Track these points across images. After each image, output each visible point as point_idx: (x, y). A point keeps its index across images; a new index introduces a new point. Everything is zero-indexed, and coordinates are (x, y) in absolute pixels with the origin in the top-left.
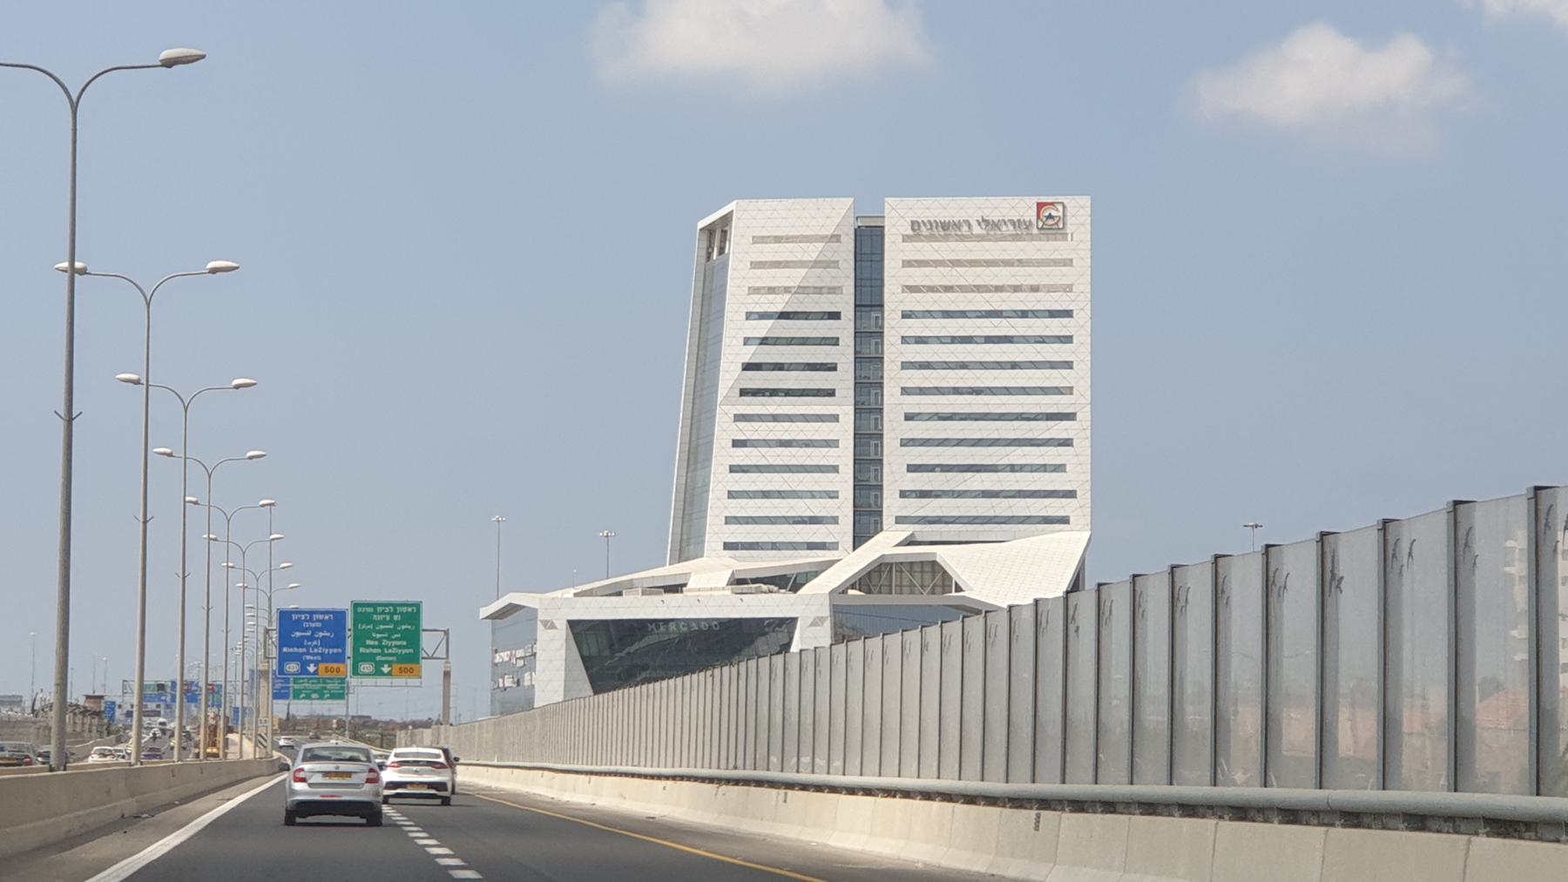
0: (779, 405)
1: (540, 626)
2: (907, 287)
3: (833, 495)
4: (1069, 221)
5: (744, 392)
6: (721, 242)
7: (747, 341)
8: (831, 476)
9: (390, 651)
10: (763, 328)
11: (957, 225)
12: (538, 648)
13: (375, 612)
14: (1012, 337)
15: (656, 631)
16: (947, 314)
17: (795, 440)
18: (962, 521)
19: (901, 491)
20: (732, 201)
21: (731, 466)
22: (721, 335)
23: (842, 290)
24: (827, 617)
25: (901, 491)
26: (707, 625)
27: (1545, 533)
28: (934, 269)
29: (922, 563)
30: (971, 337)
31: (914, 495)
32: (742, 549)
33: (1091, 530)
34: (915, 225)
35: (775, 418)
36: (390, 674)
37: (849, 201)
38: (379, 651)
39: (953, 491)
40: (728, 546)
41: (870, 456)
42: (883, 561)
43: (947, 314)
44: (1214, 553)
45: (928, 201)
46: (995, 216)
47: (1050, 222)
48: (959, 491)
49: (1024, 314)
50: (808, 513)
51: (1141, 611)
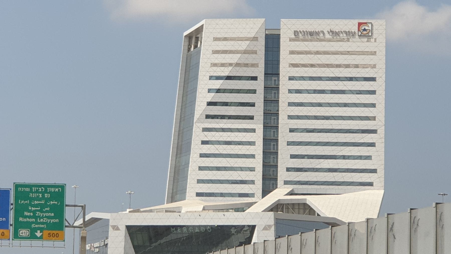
1: (110, 229)
2: (291, 64)
3: (252, 169)
4: (375, 32)
5: (208, 117)
7: (210, 91)
9: (42, 220)
10: (218, 84)
11: (318, 33)
12: (109, 241)
13: (31, 191)
15: (175, 231)
16: (312, 79)
19: (287, 168)
22: (196, 88)
24: (272, 225)
25: (287, 168)
26: (204, 229)
27: (413, 225)
28: (306, 55)
29: (299, 204)
31: (294, 170)
32: (205, 196)
33: (384, 189)
34: (296, 33)
35: (223, 130)
36: (41, 238)
37: (264, 19)
40: (198, 195)
41: (270, 150)
42: (279, 203)
43: (312, 79)
44: (366, 218)
46: (337, 29)
47: (365, 32)
49: (351, 79)
50: (240, 179)
51: (335, 240)
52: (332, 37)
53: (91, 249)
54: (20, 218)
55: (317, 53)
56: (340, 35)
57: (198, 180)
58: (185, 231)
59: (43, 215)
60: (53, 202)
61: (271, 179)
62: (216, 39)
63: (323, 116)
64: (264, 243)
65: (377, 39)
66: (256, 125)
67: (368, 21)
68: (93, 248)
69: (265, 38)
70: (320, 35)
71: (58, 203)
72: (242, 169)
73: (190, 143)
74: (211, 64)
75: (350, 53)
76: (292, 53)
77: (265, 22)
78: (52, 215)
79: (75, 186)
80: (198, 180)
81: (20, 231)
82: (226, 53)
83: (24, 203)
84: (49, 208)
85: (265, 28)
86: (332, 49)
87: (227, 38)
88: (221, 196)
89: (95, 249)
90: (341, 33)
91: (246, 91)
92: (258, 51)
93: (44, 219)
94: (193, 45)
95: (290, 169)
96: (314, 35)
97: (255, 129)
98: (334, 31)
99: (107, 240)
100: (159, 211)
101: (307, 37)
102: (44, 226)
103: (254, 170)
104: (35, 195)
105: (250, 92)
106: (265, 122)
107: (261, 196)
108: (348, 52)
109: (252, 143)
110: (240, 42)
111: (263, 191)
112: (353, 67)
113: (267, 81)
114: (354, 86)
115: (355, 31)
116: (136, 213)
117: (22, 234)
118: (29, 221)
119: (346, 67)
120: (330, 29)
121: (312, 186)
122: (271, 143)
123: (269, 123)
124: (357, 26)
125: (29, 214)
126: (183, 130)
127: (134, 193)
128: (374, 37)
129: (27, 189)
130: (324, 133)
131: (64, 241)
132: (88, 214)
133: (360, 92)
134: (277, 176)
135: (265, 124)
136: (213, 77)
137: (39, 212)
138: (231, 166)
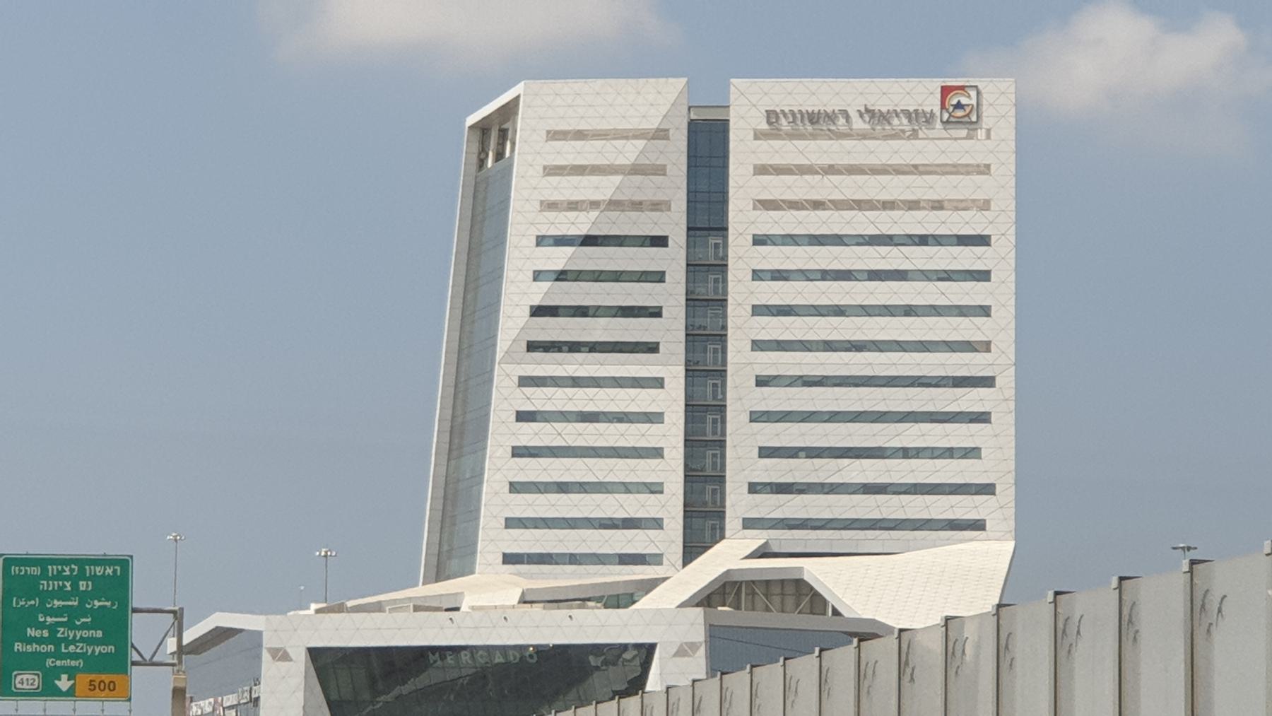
0: (581, 365)
1: (266, 656)
2: (759, 201)
3: (655, 489)
4: (986, 111)
5: (532, 347)
6: (498, 144)
7: (538, 276)
8: (653, 462)
9: (72, 648)
10: (560, 258)
11: (831, 117)
12: (263, 691)
13: (44, 575)
14: (906, 272)
15: (439, 663)
17: (603, 413)
18: (834, 526)
20: (520, 82)
21: (513, 448)
22: (502, 268)
23: (670, 206)
24: (701, 643)
29: (782, 581)
30: (850, 272)
34: (772, 116)
35: (576, 382)
36: (71, 693)
37: (684, 80)
38: (51, 648)
39: (822, 485)
40: (509, 559)
42: (727, 580)
45: (790, 84)
46: (883, 106)
47: (960, 113)
48: (832, 484)
49: (923, 240)
51: (1008, 658)
52: (869, 127)
53: (216, 710)
54: (16, 644)
55: (831, 170)
56: (891, 122)
57: (507, 519)
58: (467, 662)
59: (75, 636)
60: (99, 601)
61: (706, 515)
62: (554, 135)
63: (849, 341)
64: (666, 695)
65: (992, 133)
66: (665, 368)
67: (968, 81)
68: (221, 708)
69: (689, 131)
70: (838, 121)
71: (113, 604)
72: (627, 488)
73: (487, 416)
74: (542, 202)
75: (921, 169)
76: (761, 170)
77: (688, 87)
78: (97, 636)
79: (174, 534)
80: (507, 519)
81: (16, 676)
82: (582, 174)
83: (27, 606)
84: (91, 616)
85: (688, 103)
86: (873, 160)
87: (586, 133)
88: (571, 563)
89: (227, 712)
90: (894, 115)
91: (639, 276)
92: (668, 168)
93: (78, 644)
94: (493, 151)
95: (759, 488)
96: (822, 123)
97: (662, 379)
98: (876, 111)
99: (258, 686)
100: (397, 606)
101: (801, 128)
102: (78, 662)
103: (661, 489)
104: (54, 585)
105: (649, 279)
106: (689, 359)
107: (680, 562)
108: (915, 166)
109: (653, 418)
110: (619, 143)
111: (684, 547)
112: (927, 207)
113: (695, 248)
114: (931, 258)
115: (932, 110)
116: (332, 615)
117: (22, 683)
118: (38, 650)
119: (910, 209)
120: (865, 105)
121: (818, 531)
122: (706, 416)
123: (700, 363)
124: (939, 96)
125: (37, 633)
126: (466, 381)
127: (335, 556)
128: (984, 126)
129: (33, 568)
130: (850, 386)
131: (129, 700)
132: (188, 629)
133: (947, 276)
134: (724, 507)
135: (690, 366)
136: (547, 239)
137: (64, 627)
138: (596, 480)
